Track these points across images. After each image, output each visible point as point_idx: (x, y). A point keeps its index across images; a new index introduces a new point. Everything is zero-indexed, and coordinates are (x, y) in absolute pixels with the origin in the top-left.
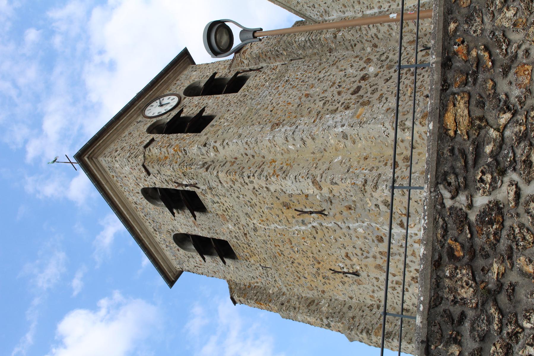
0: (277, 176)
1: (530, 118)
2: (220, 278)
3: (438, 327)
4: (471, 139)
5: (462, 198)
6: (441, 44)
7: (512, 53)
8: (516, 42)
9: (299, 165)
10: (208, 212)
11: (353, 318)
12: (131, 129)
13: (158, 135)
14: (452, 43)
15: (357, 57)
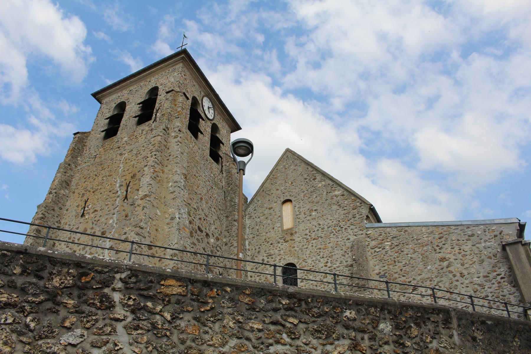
0: (153, 173)
1: (165, 331)
2: (93, 127)
3: (35, 261)
4: (157, 294)
5: (120, 285)
6: (219, 281)
7: (207, 323)
8: (213, 326)
9: (159, 187)
10: (137, 126)
11: (54, 210)
12: (197, 86)
13: (190, 103)
14: (218, 288)
15: (221, 232)
